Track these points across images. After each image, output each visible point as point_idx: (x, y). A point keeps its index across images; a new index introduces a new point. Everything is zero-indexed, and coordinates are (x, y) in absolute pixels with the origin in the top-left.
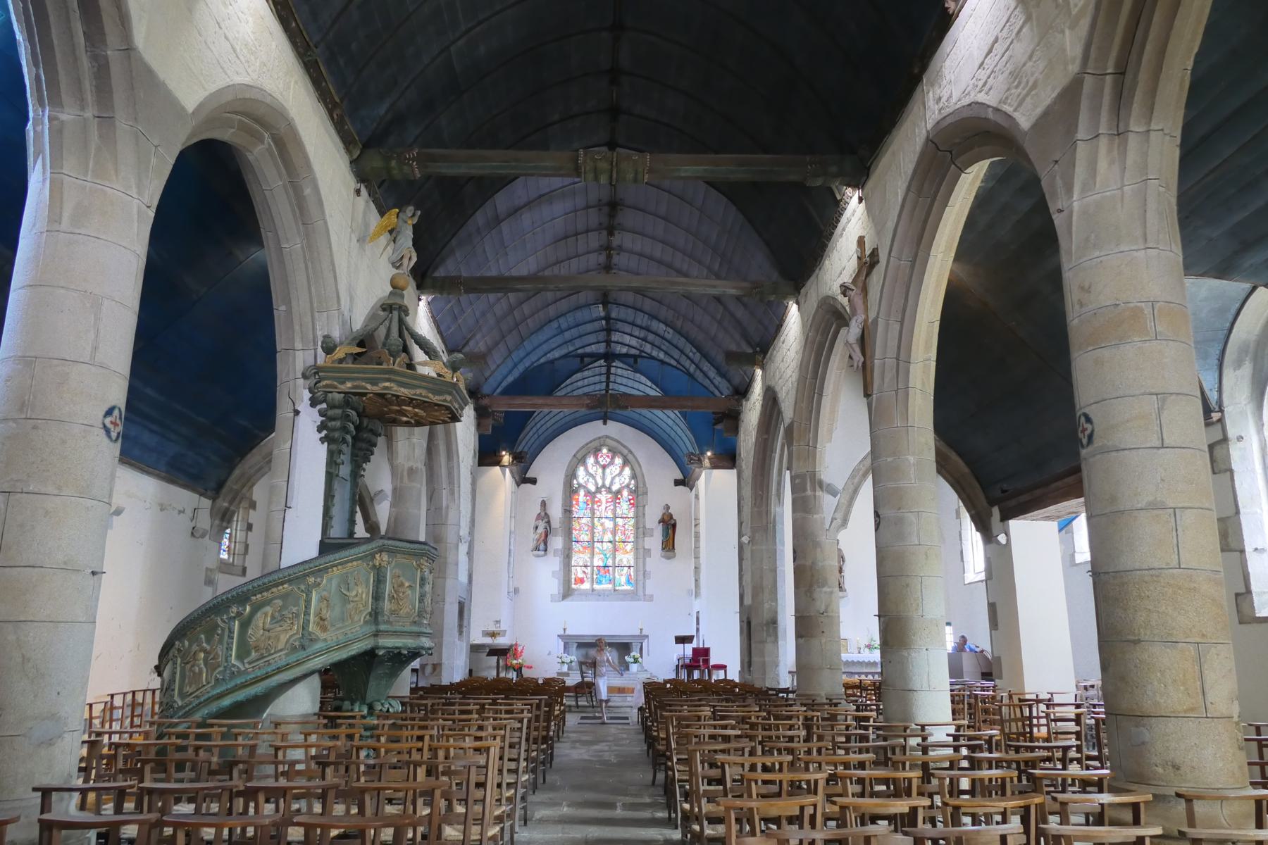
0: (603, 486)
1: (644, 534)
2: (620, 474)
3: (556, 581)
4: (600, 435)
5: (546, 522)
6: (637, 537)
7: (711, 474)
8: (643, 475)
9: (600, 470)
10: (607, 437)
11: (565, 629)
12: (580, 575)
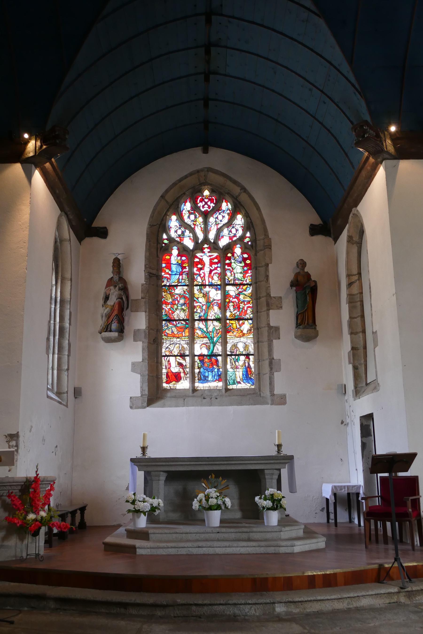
0: (206, 240)
1: (268, 304)
2: (229, 224)
3: (138, 377)
4: (200, 167)
5: (120, 289)
6: (256, 311)
7: (396, 167)
8: (263, 221)
9: (200, 220)
10: (210, 170)
11: (144, 449)
12: (175, 369)
